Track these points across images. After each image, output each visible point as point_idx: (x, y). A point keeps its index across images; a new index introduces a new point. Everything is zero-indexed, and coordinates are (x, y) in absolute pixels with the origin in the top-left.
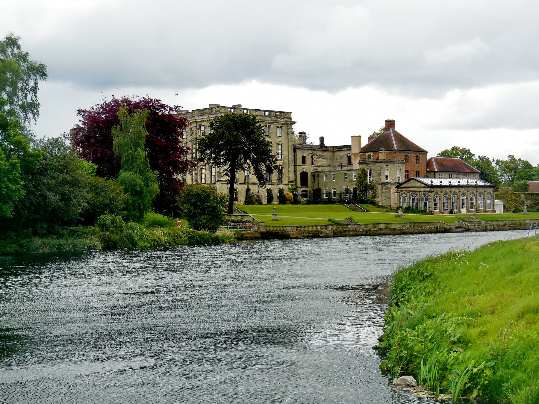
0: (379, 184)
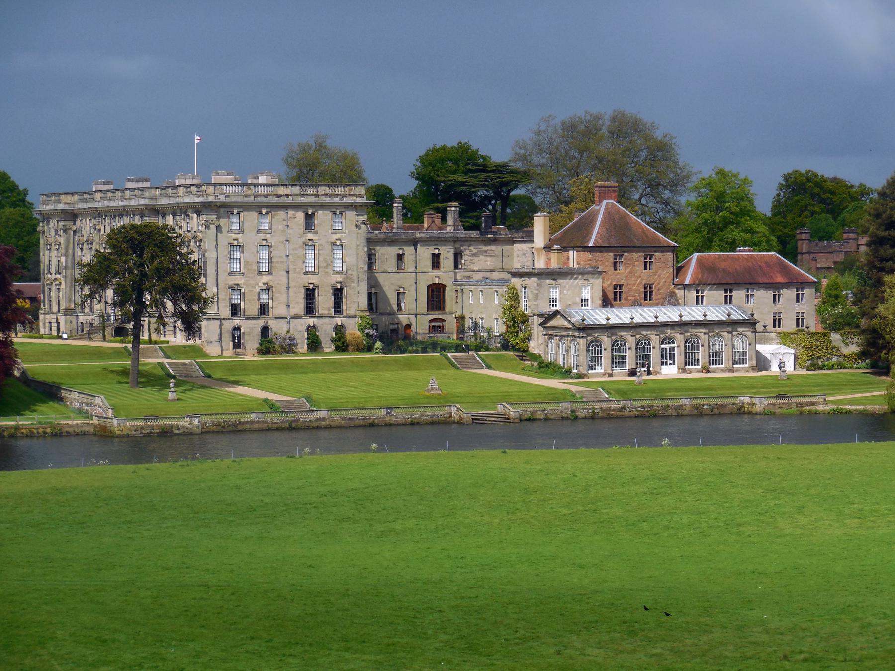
0: (534, 315)
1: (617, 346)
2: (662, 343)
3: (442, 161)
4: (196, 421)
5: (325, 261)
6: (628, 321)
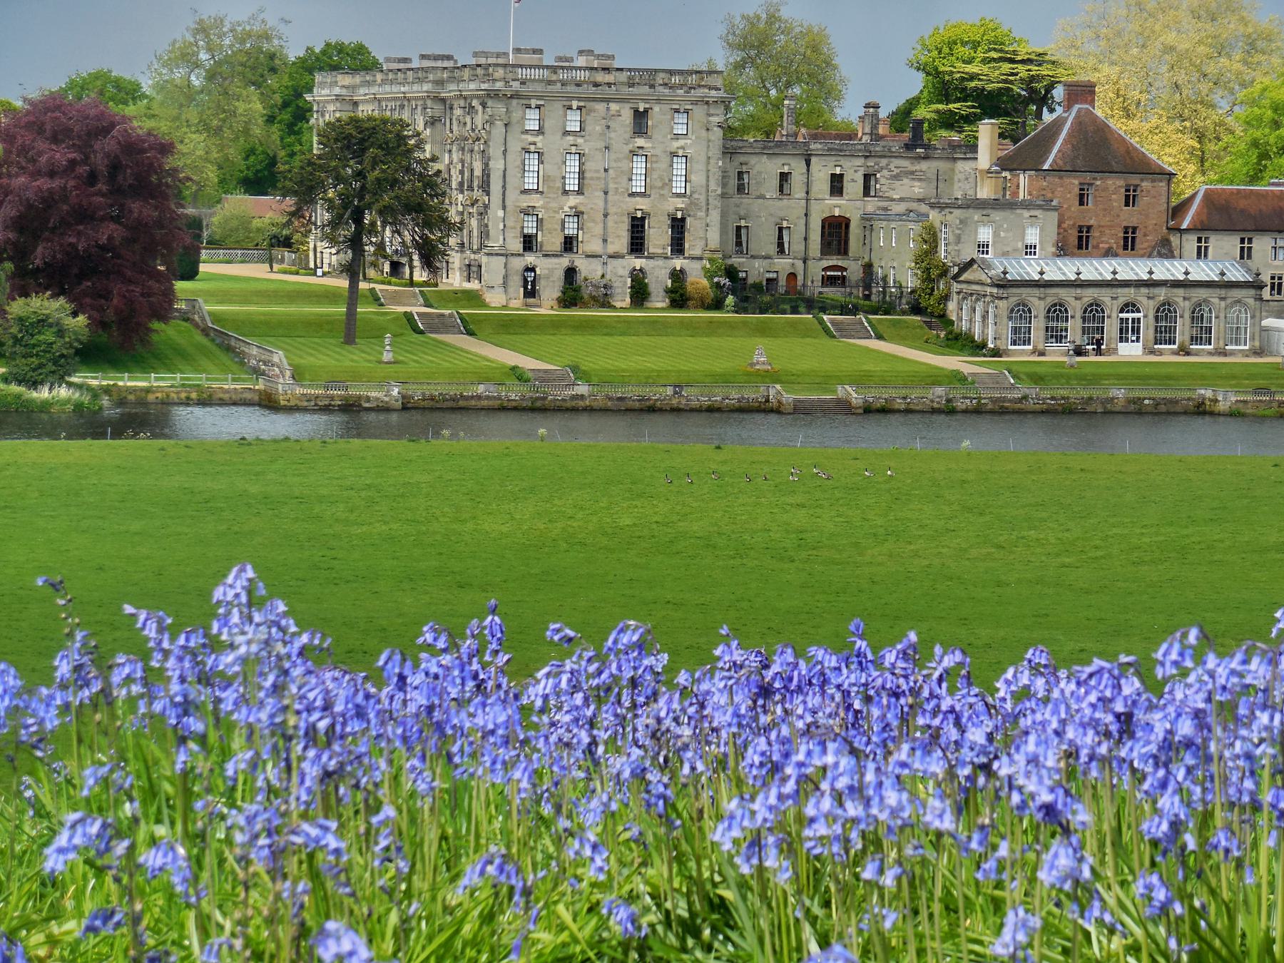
1: (1057, 312)
2: (1122, 311)
3: (952, 44)
4: (395, 392)
5: (661, 178)
6: (1073, 277)
